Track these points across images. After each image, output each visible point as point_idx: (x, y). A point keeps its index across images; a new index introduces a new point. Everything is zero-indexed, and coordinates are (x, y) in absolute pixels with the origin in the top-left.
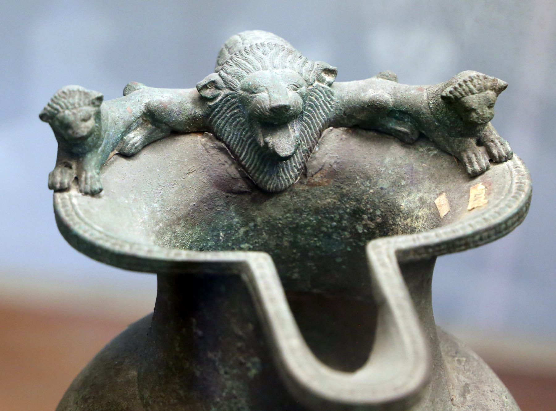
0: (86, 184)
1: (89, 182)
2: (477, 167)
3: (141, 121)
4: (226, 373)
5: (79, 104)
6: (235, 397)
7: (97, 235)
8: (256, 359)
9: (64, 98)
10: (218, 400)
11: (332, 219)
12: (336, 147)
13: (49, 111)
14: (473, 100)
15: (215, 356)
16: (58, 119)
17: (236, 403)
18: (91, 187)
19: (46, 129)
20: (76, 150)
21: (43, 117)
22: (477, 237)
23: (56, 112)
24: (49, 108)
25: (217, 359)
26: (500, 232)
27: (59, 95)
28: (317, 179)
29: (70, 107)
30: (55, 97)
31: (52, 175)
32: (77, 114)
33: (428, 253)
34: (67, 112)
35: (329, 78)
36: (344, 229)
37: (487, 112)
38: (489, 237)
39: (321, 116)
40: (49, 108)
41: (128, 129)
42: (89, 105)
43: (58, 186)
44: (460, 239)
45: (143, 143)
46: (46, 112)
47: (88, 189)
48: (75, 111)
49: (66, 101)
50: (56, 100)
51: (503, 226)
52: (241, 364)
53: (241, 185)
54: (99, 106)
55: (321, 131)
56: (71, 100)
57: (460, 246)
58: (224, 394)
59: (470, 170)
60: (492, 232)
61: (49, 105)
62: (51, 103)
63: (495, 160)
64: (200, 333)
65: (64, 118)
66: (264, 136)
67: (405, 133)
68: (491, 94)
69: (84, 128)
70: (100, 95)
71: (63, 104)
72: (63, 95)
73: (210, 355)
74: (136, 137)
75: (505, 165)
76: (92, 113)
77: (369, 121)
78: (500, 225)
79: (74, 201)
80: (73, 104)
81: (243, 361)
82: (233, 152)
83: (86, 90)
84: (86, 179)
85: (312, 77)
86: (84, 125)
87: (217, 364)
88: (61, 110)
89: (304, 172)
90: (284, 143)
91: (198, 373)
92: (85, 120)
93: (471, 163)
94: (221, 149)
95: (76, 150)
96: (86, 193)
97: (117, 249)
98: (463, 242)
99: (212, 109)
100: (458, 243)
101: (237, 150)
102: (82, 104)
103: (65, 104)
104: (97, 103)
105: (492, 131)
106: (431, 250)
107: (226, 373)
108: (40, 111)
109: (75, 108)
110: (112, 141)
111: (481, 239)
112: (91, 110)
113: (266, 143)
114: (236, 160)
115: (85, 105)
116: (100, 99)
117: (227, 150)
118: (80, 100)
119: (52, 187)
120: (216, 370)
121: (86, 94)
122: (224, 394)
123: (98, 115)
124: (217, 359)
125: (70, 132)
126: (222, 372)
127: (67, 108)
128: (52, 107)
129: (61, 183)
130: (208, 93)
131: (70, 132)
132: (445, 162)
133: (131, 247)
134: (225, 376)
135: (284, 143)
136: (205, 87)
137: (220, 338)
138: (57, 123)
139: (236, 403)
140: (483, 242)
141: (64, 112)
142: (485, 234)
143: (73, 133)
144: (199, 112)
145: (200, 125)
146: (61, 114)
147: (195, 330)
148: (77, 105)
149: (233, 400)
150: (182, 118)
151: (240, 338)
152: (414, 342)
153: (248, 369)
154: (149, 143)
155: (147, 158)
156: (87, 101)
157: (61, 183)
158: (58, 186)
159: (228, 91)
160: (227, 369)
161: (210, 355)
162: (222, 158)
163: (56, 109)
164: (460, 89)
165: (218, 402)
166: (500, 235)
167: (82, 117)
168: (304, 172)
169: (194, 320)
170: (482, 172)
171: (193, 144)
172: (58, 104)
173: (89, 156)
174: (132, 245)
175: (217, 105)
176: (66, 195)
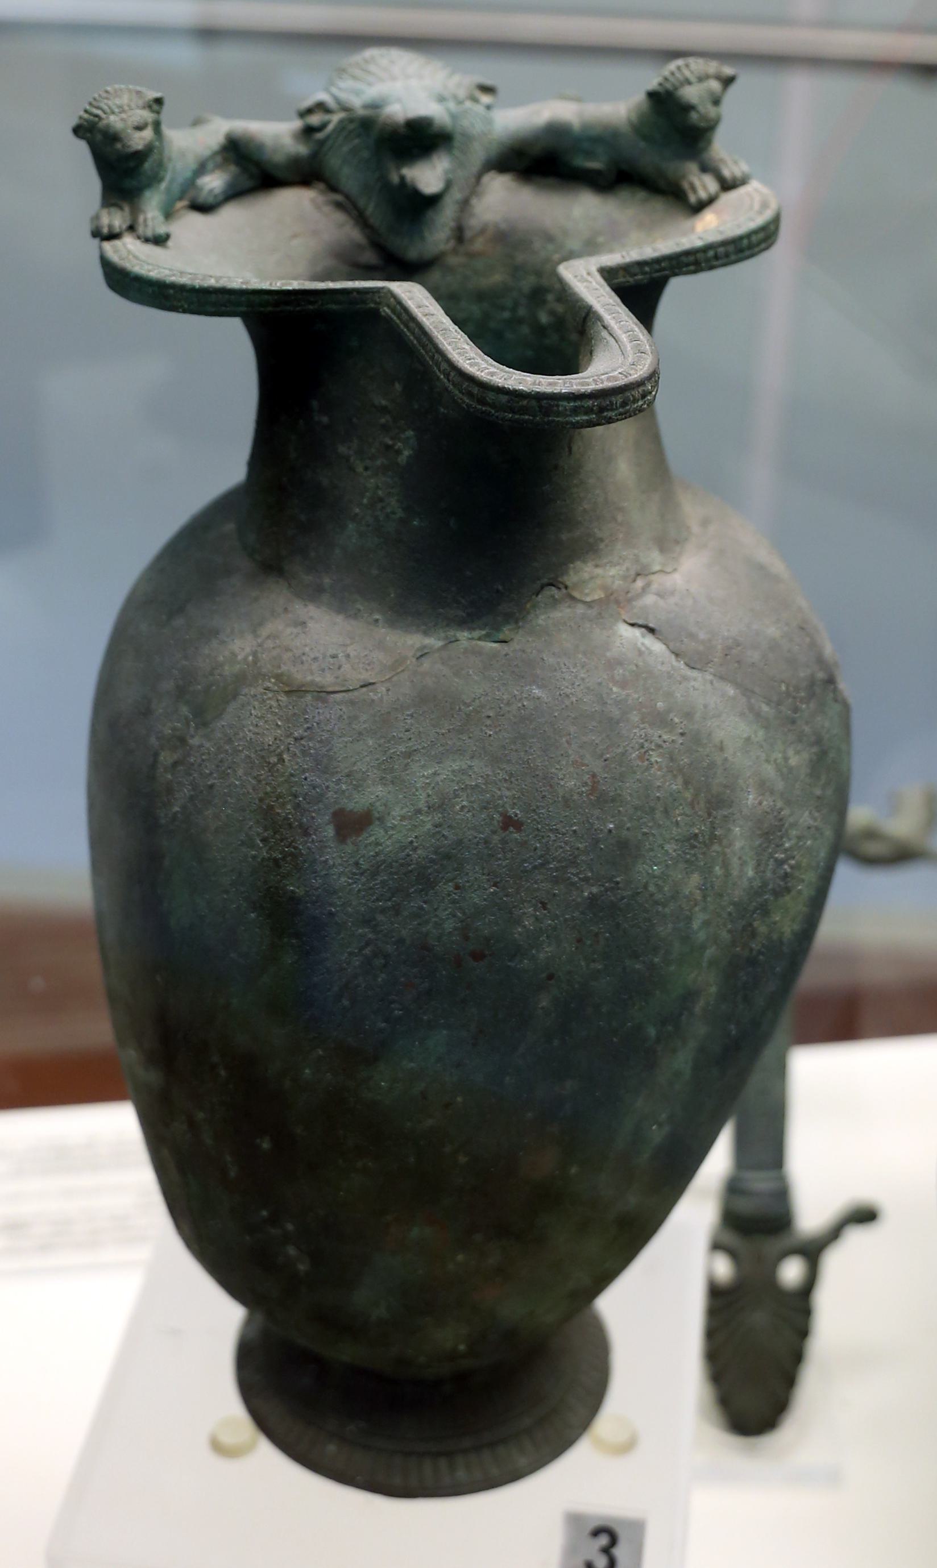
0: (146, 226)
1: (150, 223)
2: (703, 195)
3: (219, 159)
4: (366, 469)
5: (129, 106)
6: (381, 500)
7: (167, 272)
8: (410, 433)
9: (107, 98)
10: (357, 510)
11: (503, 308)
12: (502, 199)
13: (86, 120)
14: (691, 94)
15: (349, 448)
16: (100, 131)
17: (383, 508)
18: (154, 230)
19: (82, 149)
20: (129, 183)
21: (78, 131)
22: (711, 253)
23: (97, 119)
24: (86, 116)
25: (351, 452)
26: (741, 251)
27: (100, 96)
28: (478, 245)
29: (117, 110)
30: (95, 99)
31: (97, 217)
32: (125, 115)
33: (644, 273)
34: (112, 118)
35: (486, 99)
36: (520, 321)
37: (712, 111)
38: (727, 255)
39: (478, 155)
40: (86, 116)
41: (202, 169)
42: (144, 108)
43: (105, 230)
44: (687, 253)
45: (224, 192)
46: (82, 121)
47: (149, 233)
48: (124, 116)
49: (110, 103)
50: (94, 103)
51: (745, 242)
52: (388, 447)
53: (370, 257)
54: (158, 113)
55: (479, 177)
56: (118, 102)
57: (687, 265)
58: (365, 501)
59: (692, 199)
60: (731, 248)
61: (86, 111)
62: (88, 107)
63: (727, 185)
64: (325, 420)
65: (108, 126)
66: (398, 168)
67: (598, 172)
68: (715, 85)
69: (139, 140)
70: (158, 95)
71: (105, 107)
72: (104, 95)
73: (342, 449)
74: (214, 182)
75: (742, 191)
76: (150, 120)
77: (543, 160)
78: (741, 238)
79: (130, 247)
80: (120, 107)
81: (390, 443)
82: (355, 206)
83: (139, 88)
84: (145, 220)
85: (462, 93)
86: (138, 135)
87: (352, 459)
88: (103, 116)
89: (459, 234)
90: (428, 176)
91: (325, 482)
92: (139, 128)
93: (694, 189)
94: (339, 205)
95: (129, 183)
96: (147, 240)
97: (197, 283)
98: (691, 258)
99: (322, 143)
100: (684, 259)
101: (361, 202)
102: (133, 105)
103: (110, 108)
104: (155, 107)
105: (722, 148)
106: (647, 269)
107: (366, 469)
108: (74, 122)
109: (123, 111)
110: (180, 180)
111: (716, 257)
112: (147, 116)
113: (402, 178)
114: (361, 220)
115: (138, 107)
116: (159, 101)
117: (348, 206)
118: (131, 100)
119: (96, 234)
120: (352, 469)
121: (138, 93)
122: (365, 501)
123: (157, 126)
124: (351, 452)
125: (119, 146)
126: (360, 469)
127: (113, 113)
128: (91, 114)
129: (110, 226)
130: (315, 120)
131: (119, 146)
132: (658, 205)
133: (217, 281)
134: (365, 474)
135: (428, 176)
136: (310, 111)
137: (355, 420)
138: (99, 137)
139: (383, 508)
140: (720, 262)
141: (108, 118)
142: (721, 250)
143: (124, 146)
144: (302, 150)
145: (305, 173)
146: (105, 122)
147: (316, 418)
148: (126, 108)
149: (379, 505)
150: (279, 158)
151: (384, 410)
152: (634, 339)
153: (399, 452)
154: (234, 194)
155: (231, 214)
156: (140, 103)
157: (110, 226)
158: (105, 230)
159: (341, 115)
160: (368, 463)
161: (342, 449)
162: (340, 217)
163: (97, 116)
164: (672, 79)
165: (356, 515)
166: (741, 255)
167: (136, 124)
168: (459, 234)
169: (315, 404)
170: (711, 201)
171: (295, 202)
172: (98, 108)
173: (147, 194)
174: (218, 279)
175: (328, 138)
176: (117, 243)
